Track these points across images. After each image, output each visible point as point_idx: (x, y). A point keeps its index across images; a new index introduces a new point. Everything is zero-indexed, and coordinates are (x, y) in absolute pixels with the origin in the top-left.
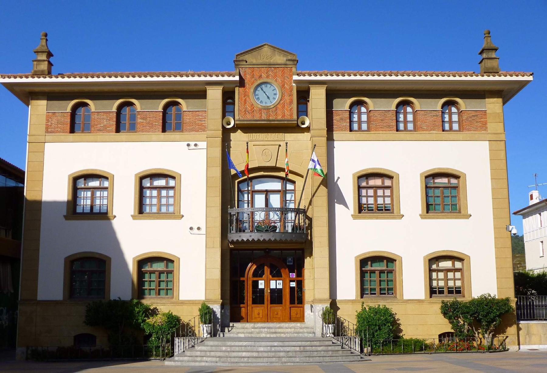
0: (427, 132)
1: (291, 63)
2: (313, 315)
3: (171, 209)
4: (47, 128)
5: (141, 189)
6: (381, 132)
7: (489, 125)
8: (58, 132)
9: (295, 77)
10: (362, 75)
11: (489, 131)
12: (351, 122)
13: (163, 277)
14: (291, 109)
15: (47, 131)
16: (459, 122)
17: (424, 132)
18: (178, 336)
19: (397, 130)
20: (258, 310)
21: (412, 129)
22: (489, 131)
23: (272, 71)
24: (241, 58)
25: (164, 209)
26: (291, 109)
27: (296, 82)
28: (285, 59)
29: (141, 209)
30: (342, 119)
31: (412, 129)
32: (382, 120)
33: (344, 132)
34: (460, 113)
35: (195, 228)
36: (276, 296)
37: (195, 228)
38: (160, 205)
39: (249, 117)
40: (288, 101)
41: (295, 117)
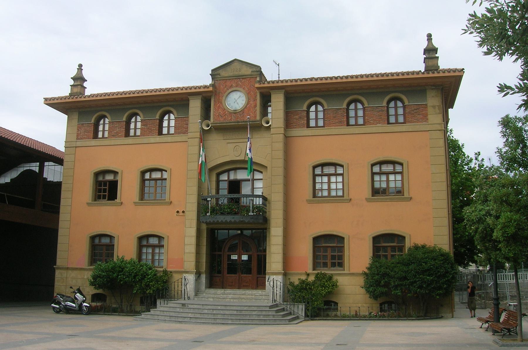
0: (374, 126)
1: (256, 73)
2: (275, 281)
3: (340, 193)
4: (77, 136)
5: (143, 180)
6: (333, 127)
7: (429, 117)
8: (84, 138)
9: (257, 85)
10: (434, 73)
11: (430, 123)
12: (348, 117)
13: (157, 250)
14: (255, 112)
15: (77, 139)
16: (404, 115)
17: (371, 126)
18: (159, 298)
19: (348, 125)
20: (233, 277)
21: (362, 123)
22: (430, 123)
23: (241, 81)
24: (216, 73)
25: (333, 193)
26: (255, 112)
27: (258, 88)
28: (251, 70)
29: (142, 197)
30: (300, 118)
31: (362, 123)
32: (334, 117)
33: (302, 129)
34: (404, 107)
35: (181, 211)
36: (246, 267)
37: (181, 211)
38: (329, 189)
39: (222, 120)
40: (253, 106)
41: (258, 118)
